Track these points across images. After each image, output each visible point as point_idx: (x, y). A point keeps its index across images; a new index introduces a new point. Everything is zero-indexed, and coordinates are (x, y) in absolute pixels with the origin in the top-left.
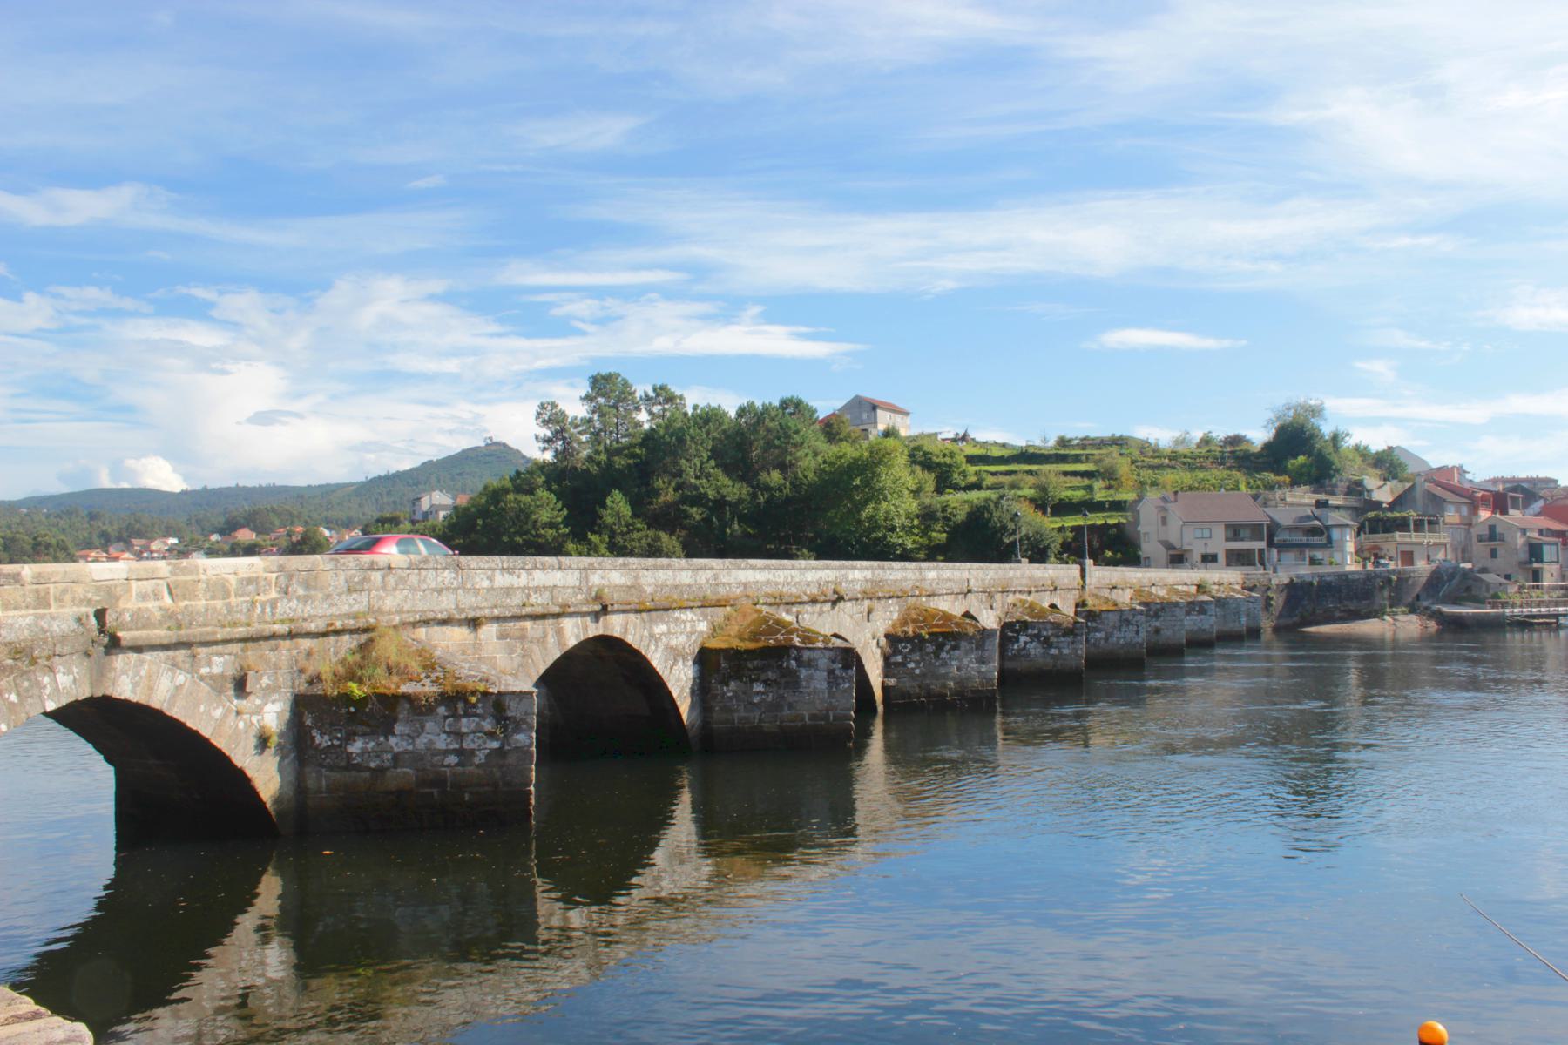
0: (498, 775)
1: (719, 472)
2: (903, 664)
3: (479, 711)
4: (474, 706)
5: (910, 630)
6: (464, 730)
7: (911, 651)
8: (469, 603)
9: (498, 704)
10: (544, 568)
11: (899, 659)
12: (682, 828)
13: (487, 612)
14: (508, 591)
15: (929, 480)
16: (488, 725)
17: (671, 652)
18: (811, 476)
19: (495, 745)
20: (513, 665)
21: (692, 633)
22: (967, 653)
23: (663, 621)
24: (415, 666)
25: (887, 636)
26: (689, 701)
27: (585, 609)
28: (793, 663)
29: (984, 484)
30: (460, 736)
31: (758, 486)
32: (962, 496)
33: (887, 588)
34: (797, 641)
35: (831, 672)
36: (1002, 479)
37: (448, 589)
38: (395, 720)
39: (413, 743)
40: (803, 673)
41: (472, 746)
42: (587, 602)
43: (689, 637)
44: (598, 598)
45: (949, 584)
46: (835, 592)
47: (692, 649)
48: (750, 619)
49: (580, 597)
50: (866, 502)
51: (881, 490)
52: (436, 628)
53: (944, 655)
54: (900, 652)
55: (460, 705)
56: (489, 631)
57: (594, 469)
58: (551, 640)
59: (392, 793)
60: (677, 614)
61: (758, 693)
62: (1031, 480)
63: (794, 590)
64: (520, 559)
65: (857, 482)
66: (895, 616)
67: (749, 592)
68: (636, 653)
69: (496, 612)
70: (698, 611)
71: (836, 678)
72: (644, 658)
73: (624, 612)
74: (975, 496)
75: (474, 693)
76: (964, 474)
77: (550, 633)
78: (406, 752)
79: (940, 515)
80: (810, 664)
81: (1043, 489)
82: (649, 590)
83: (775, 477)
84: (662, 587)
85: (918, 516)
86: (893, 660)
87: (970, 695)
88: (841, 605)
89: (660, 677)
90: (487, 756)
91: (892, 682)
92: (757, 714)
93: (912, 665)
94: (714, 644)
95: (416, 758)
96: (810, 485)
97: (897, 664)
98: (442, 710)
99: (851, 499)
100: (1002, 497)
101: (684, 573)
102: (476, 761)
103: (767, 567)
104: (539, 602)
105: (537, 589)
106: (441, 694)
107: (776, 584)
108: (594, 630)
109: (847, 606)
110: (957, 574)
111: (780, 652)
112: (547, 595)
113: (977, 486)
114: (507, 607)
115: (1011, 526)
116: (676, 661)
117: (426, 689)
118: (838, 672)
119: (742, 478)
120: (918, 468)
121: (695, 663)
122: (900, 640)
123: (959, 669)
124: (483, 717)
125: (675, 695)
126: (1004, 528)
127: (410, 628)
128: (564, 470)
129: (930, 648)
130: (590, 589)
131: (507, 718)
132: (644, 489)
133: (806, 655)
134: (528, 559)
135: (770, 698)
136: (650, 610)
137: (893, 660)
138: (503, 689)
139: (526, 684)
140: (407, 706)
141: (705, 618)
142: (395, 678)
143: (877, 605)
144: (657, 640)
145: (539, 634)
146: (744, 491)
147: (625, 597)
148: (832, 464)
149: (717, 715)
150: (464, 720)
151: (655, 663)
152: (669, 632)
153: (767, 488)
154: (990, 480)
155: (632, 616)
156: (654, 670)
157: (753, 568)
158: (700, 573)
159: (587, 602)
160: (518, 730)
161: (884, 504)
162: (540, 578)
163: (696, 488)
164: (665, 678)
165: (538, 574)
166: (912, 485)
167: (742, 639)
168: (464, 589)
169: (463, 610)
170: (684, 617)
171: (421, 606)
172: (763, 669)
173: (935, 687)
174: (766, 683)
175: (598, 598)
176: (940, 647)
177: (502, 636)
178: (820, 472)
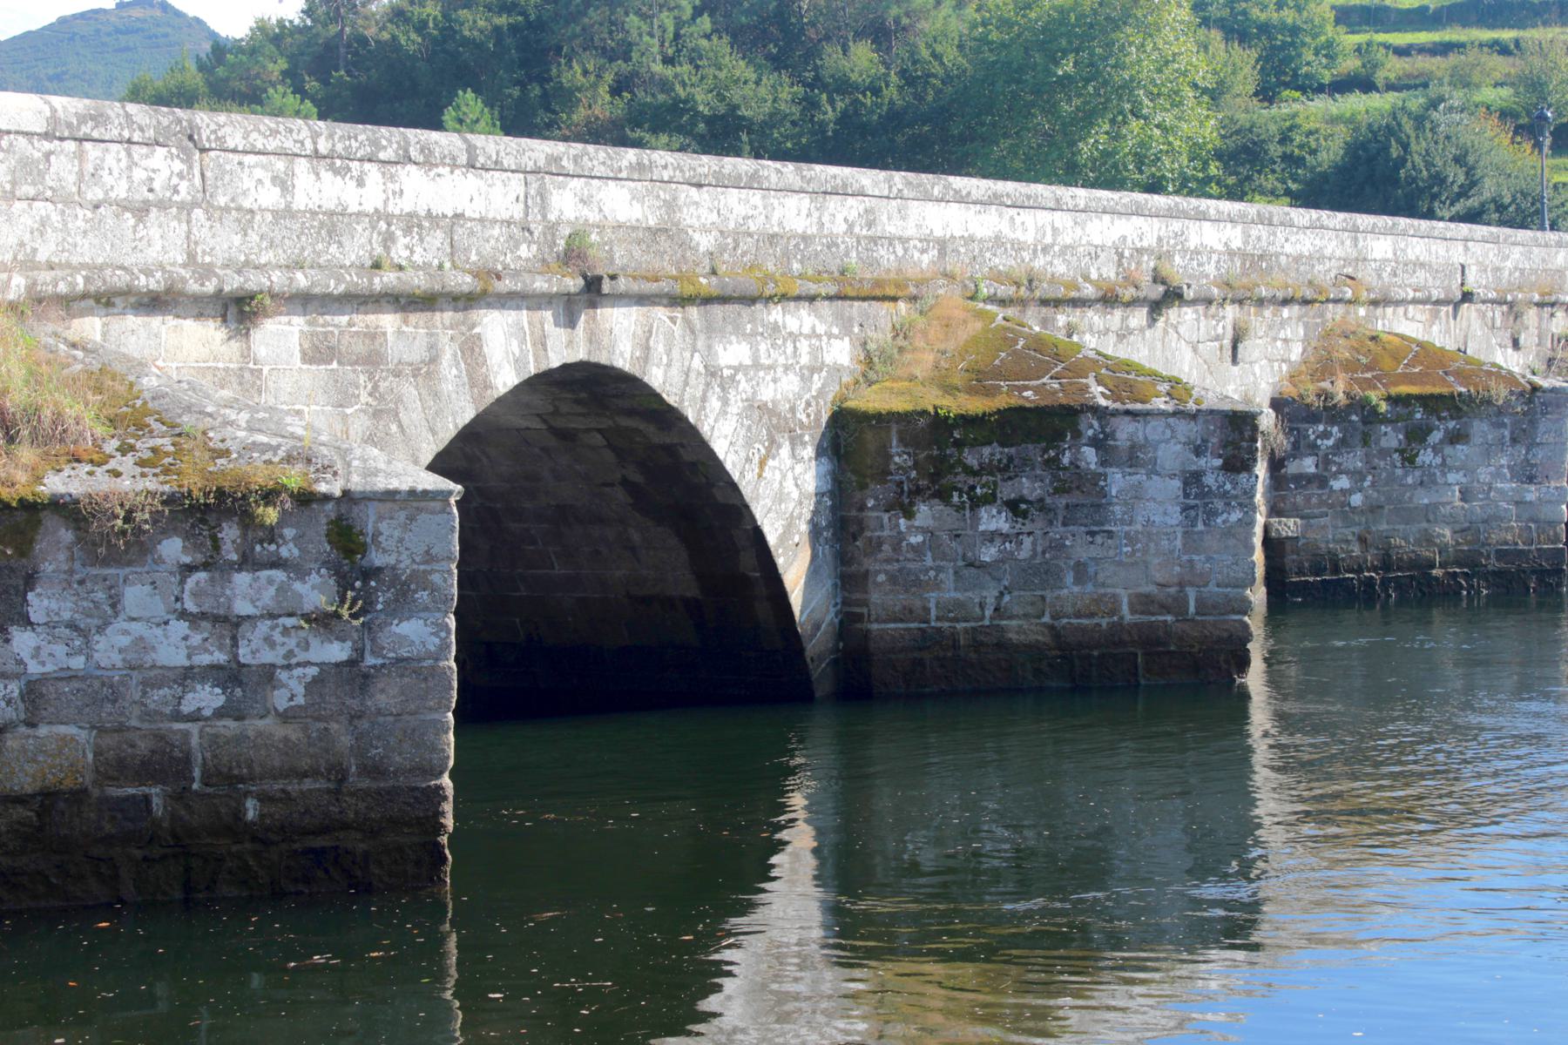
0: (346, 741)
1: (722, 45)
2: (1321, 481)
3: (287, 551)
4: (272, 534)
5: (1339, 389)
6: (242, 608)
7: (1342, 443)
8: (226, 252)
9: (344, 531)
10: (428, 162)
11: (1308, 465)
12: (792, 900)
13: (277, 279)
14: (333, 223)
15: (1245, 64)
16: (315, 593)
17: (760, 417)
18: (951, 54)
19: (337, 652)
20: (379, 426)
21: (813, 370)
22: (1488, 452)
23: (738, 330)
24: (84, 416)
25: (1276, 404)
26: (805, 555)
27: (540, 284)
28: (1090, 455)
29: (1380, 77)
30: (230, 625)
31: (817, 82)
32: (1321, 105)
33: (1278, 277)
34: (1098, 394)
35: (1192, 479)
36: (1423, 63)
37: (163, 205)
38: (30, 580)
39: (87, 650)
40: (1117, 481)
41: (268, 657)
42: (544, 266)
43: (806, 379)
44: (573, 254)
45: (1421, 276)
46: (1158, 279)
47: (814, 416)
48: (963, 335)
49: (524, 251)
50: (1087, 118)
51: (1127, 88)
52: (132, 321)
53: (1426, 457)
54: (1313, 448)
55: (230, 533)
56: (280, 336)
57: (411, 41)
58: (450, 371)
59: (20, 800)
60: (776, 314)
61: (992, 537)
62: (1501, 66)
63: (1060, 268)
64: (363, 133)
65: (1067, 67)
66: (1296, 353)
67: (951, 264)
68: (666, 416)
69: (302, 281)
70: (825, 307)
71: (1205, 494)
72: (692, 433)
73: (642, 299)
74: (1355, 103)
75: (269, 496)
76: (1329, 51)
77: (449, 352)
78: (70, 676)
79: (1275, 150)
80: (1134, 458)
81: (1535, 85)
82: (705, 242)
83: (861, 59)
84: (740, 234)
85: (1219, 155)
86: (1292, 468)
87: (1494, 564)
88: (1172, 313)
89: (734, 487)
90: (313, 686)
91: (1289, 527)
92: (990, 595)
93: (1342, 483)
94: (871, 400)
95: (99, 692)
96: (948, 79)
97: (1302, 480)
98: (173, 549)
99: (1051, 110)
100: (1433, 104)
101: (792, 201)
102: (280, 699)
103: (995, 200)
104: (419, 259)
105: (412, 222)
106: (170, 500)
107: (1019, 247)
108: (564, 348)
109: (1184, 317)
110: (1439, 248)
111: (1042, 428)
112: (437, 239)
113: (1365, 84)
114: (334, 269)
115: (1456, 176)
116: (773, 445)
117: (126, 484)
118: (1209, 480)
119: (778, 63)
120: (1216, 35)
121: (820, 452)
122: (1313, 417)
123: (1465, 495)
124: (296, 569)
125: (772, 539)
126: (1439, 179)
127: (55, 312)
128: (330, 47)
129: (1391, 438)
130: (552, 228)
131: (369, 573)
132: (535, 91)
133: (1125, 431)
134: (396, 134)
135: (1024, 554)
136: (707, 300)
137: (1292, 468)
138: (357, 483)
139: (410, 473)
140: (67, 535)
141: (846, 330)
142: (27, 453)
143: (1259, 321)
144: (727, 384)
145: (416, 352)
146: (785, 94)
147: (641, 257)
148: (1005, 24)
149: (880, 597)
150: (242, 579)
151: (720, 448)
152: (757, 365)
153: (843, 86)
154: (1394, 67)
155: (661, 313)
156: (718, 465)
157: (962, 199)
158: (833, 203)
159: (544, 266)
160: (403, 604)
161: (1135, 125)
162: (421, 190)
163: (665, 86)
164: (747, 491)
165: (411, 177)
166: (1203, 74)
167: (949, 389)
168: (209, 209)
169: (207, 271)
170: (792, 324)
171: (88, 250)
172: (1006, 469)
173: (1404, 542)
174: (1014, 507)
175: (573, 254)
176: (1417, 435)
177: (318, 352)
178: (974, 46)
